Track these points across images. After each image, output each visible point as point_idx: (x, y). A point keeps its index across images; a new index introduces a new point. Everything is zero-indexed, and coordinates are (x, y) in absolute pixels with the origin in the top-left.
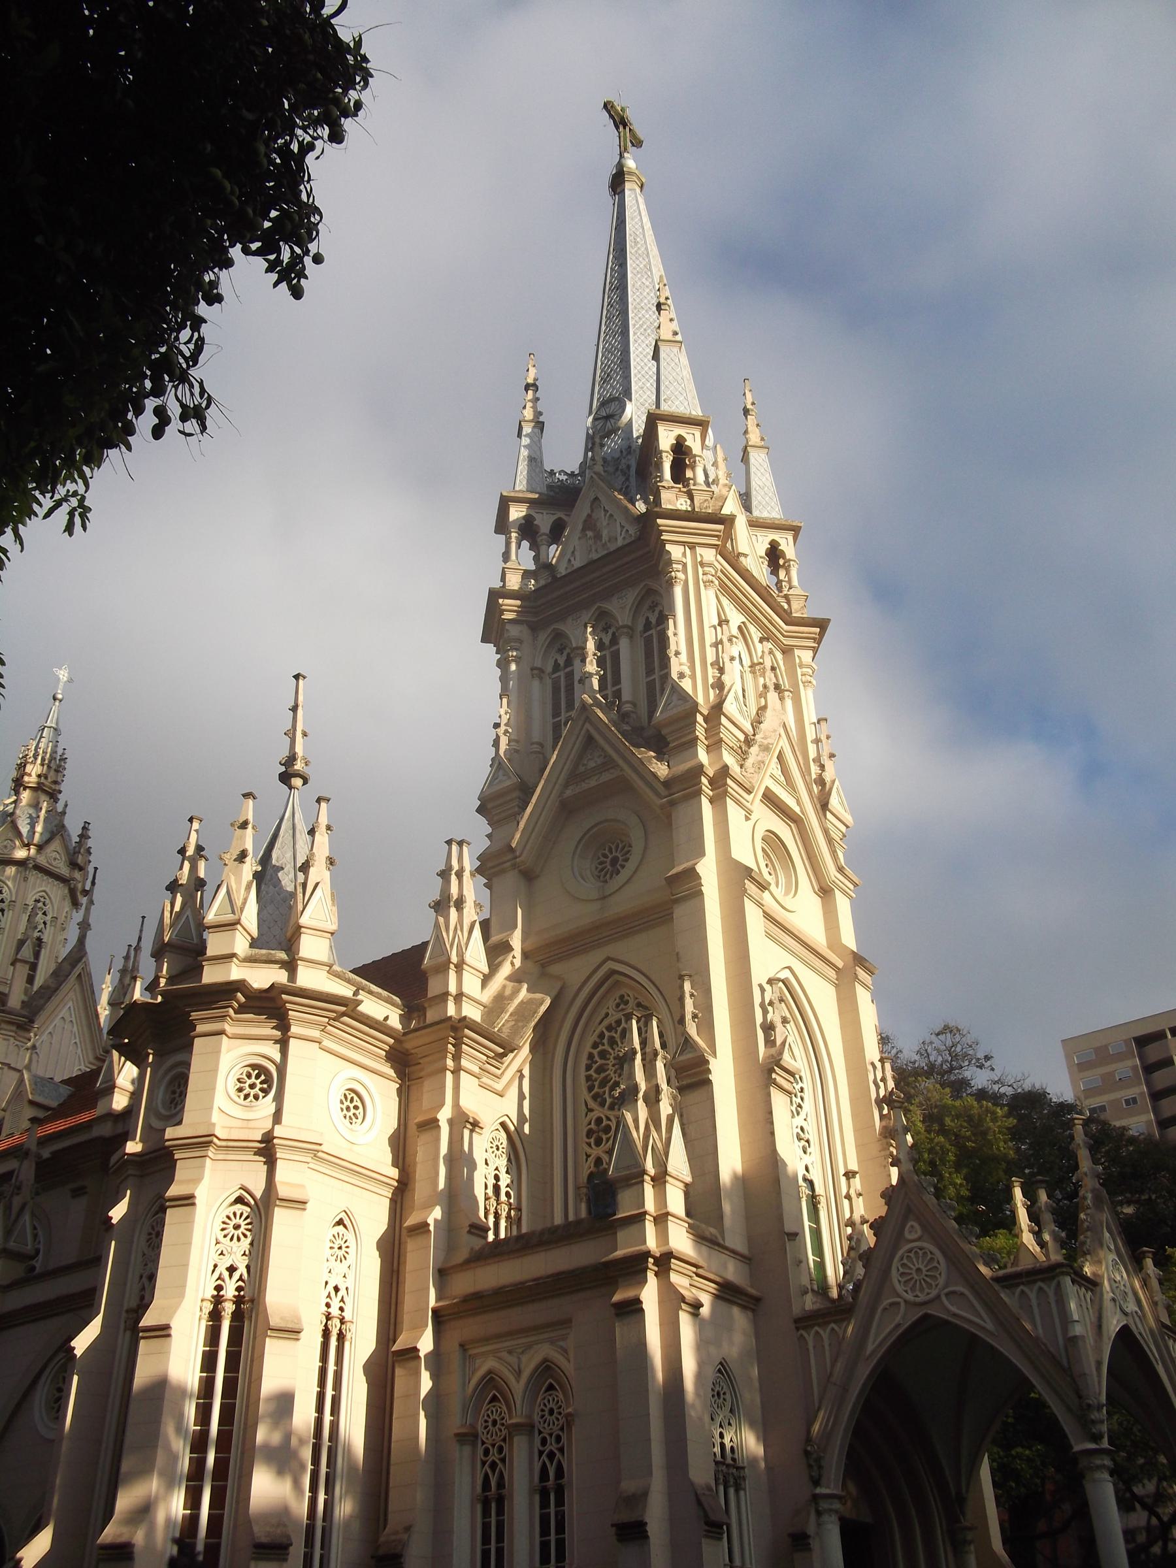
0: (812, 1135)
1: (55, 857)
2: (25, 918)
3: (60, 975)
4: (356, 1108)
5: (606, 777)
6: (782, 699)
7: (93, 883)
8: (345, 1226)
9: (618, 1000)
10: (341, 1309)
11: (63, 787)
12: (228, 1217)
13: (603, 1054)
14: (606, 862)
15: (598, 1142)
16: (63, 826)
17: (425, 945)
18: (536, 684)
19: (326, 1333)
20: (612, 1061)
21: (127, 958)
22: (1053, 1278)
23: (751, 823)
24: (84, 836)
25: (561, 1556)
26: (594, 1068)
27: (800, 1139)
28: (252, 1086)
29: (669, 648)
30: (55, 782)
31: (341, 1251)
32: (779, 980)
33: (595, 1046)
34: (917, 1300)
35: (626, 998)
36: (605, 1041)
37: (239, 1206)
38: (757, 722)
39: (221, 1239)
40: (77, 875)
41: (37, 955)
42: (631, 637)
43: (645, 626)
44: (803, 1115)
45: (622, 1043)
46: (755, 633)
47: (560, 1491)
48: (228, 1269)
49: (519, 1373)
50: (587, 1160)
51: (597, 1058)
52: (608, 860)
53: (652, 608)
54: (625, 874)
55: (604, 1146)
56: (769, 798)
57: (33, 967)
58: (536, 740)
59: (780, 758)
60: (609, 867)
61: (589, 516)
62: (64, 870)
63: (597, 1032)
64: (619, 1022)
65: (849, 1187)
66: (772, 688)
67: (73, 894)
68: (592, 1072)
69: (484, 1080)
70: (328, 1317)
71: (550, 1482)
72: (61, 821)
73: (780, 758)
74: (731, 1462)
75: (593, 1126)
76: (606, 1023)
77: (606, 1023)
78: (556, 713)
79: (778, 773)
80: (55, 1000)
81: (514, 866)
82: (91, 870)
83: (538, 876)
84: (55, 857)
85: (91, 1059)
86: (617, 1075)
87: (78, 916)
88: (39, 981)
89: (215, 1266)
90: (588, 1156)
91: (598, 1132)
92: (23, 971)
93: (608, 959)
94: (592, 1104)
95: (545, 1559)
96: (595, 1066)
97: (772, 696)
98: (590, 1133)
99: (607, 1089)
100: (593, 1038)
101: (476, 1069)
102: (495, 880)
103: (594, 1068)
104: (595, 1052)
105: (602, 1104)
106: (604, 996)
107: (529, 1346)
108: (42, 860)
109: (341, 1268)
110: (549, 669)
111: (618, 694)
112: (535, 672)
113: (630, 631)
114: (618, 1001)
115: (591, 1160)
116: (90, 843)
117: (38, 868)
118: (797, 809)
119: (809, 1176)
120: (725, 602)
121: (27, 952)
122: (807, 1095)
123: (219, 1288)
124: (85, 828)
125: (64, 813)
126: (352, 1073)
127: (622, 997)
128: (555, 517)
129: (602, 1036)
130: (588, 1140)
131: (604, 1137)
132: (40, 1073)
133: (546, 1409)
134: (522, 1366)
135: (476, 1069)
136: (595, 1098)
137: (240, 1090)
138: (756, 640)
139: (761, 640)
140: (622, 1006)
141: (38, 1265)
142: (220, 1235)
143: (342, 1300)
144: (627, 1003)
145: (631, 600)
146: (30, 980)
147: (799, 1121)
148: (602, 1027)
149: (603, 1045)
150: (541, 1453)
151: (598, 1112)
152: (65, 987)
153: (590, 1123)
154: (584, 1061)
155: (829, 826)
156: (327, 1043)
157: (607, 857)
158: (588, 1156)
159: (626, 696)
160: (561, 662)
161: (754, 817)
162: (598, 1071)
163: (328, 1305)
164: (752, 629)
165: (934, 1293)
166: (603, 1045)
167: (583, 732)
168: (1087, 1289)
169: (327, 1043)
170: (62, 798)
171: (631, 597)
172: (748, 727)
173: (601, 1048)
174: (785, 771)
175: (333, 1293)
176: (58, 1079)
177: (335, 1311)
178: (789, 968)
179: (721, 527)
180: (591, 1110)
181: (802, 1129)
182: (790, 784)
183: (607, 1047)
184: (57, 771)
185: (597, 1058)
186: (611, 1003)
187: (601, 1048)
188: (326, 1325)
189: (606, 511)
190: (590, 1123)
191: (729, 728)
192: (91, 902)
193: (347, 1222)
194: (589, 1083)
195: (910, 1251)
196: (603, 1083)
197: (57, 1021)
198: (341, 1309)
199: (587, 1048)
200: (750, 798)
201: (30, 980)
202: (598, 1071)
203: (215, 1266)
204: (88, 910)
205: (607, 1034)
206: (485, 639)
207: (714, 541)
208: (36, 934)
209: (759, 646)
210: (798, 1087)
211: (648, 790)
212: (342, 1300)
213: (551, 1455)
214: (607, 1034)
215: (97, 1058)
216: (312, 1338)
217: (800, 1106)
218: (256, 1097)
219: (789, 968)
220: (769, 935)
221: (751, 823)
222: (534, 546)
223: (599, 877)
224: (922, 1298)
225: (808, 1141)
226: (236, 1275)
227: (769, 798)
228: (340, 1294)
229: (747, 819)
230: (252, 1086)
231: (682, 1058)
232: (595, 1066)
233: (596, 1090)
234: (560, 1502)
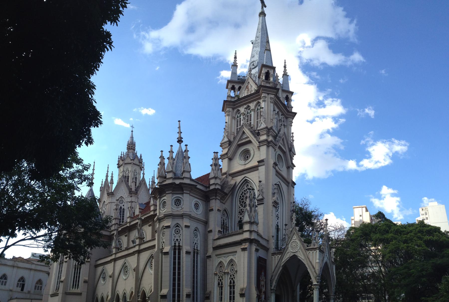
0: (279, 216)
1: (136, 161)
2: (133, 173)
3: (140, 183)
4: (197, 207)
5: (247, 140)
6: (285, 127)
7: (144, 165)
8: (197, 231)
10: (197, 248)
11: (136, 148)
12: (176, 230)
13: (243, 196)
15: (241, 214)
16: (137, 156)
17: (209, 173)
18: (233, 120)
19: (194, 253)
20: (245, 198)
21: (152, 179)
22: (316, 250)
23: (276, 152)
24: (141, 157)
25: (234, 299)
27: (277, 217)
28: (178, 203)
29: (256, 288)
30: (134, 147)
31: (196, 236)
32: (277, 184)
33: (241, 194)
34: (293, 252)
37: (177, 227)
38: (278, 133)
39: (175, 234)
40: (141, 164)
41: (136, 180)
42: (254, 112)
44: (278, 212)
46: (280, 113)
47: (234, 286)
48: (176, 240)
49: (226, 262)
51: (242, 197)
53: (259, 106)
54: (249, 160)
55: (242, 215)
56: (280, 148)
57: (136, 183)
58: (233, 132)
59: (283, 139)
61: (247, 86)
62: (138, 164)
64: (246, 190)
65: (285, 227)
66: (283, 125)
67: (140, 167)
68: (240, 200)
69: (221, 201)
70: (194, 249)
71: (232, 284)
72: (136, 155)
73: (283, 139)
75: (240, 211)
76: (244, 190)
79: (282, 142)
80: (141, 189)
81: (227, 157)
82: (143, 163)
84: (136, 161)
85: (148, 199)
87: (142, 172)
88: (137, 185)
89: (174, 239)
90: (239, 217)
92: (134, 183)
95: (230, 299)
96: (241, 199)
97: (283, 127)
98: (239, 212)
100: (241, 193)
101: (219, 199)
102: (223, 160)
104: (241, 196)
105: (242, 206)
106: (244, 185)
107: (228, 256)
108: (134, 162)
109: (196, 239)
110: (236, 117)
111: (251, 123)
112: (234, 118)
113: (254, 110)
115: (239, 218)
116: (142, 158)
117: (134, 164)
118: (285, 150)
119: (278, 224)
120: (275, 106)
121: (134, 180)
122: (280, 208)
123: (175, 244)
124: (141, 155)
125: (137, 153)
126: (195, 200)
127: (247, 185)
128: (239, 86)
129: (243, 192)
131: (242, 213)
132: (141, 202)
134: (227, 260)
135: (219, 199)
136: (241, 205)
137: (177, 205)
138: (280, 115)
139: (281, 115)
141: (145, 240)
142: (174, 233)
143: (197, 246)
145: (255, 104)
146: (136, 185)
147: (277, 213)
150: (230, 278)
152: (142, 186)
154: (239, 197)
155: (291, 154)
156: (191, 194)
158: (239, 217)
159: (252, 122)
160: (239, 116)
161: (276, 151)
163: (194, 247)
164: (280, 112)
165: (297, 251)
168: (322, 253)
169: (191, 194)
170: (136, 150)
171: (255, 103)
172: (277, 132)
173: (243, 195)
174: (283, 142)
175: (195, 245)
176: (143, 203)
177: (196, 248)
178: (279, 182)
179: (276, 91)
180: (240, 208)
181: (278, 215)
182: (284, 145)
183: (244, 195)
184: (134, 145)
185: (242, 197)
186: (245, 186)
187: (243, 195)
188: (194, 251)
189: (251, 85)
192: (144, 169)
193: (197, 230)
195: (293, 242)
196: (243, 202)
197: (141, 193)
198: (197, 248)
199: (240, 195)
200: (276, 147)
201: (136, 185)
203: (174, 239)
204: (144, 171)
208: (135, 176)
209: (281, 116)
210: (278, 206)
211: (255, 143)
212: (197, 246)
213: (232, 279)
214: (244, 192)
215: (150, 199)
216: (192, 254)
217: (278, 210)
218: (179, 205)
219: (279, 182)
220: (276, 175)
221: (276, 152)
222: (234, 92)
224: (294, 251)
225: (278, 217)
226: (178, 241)
227: (280, 148)
228: (196, 245)
229: (275, 151)
230: (178, 203)
231: (258, 198)
232: (241, 199)
233: (241, 203)
234: (234, 288)
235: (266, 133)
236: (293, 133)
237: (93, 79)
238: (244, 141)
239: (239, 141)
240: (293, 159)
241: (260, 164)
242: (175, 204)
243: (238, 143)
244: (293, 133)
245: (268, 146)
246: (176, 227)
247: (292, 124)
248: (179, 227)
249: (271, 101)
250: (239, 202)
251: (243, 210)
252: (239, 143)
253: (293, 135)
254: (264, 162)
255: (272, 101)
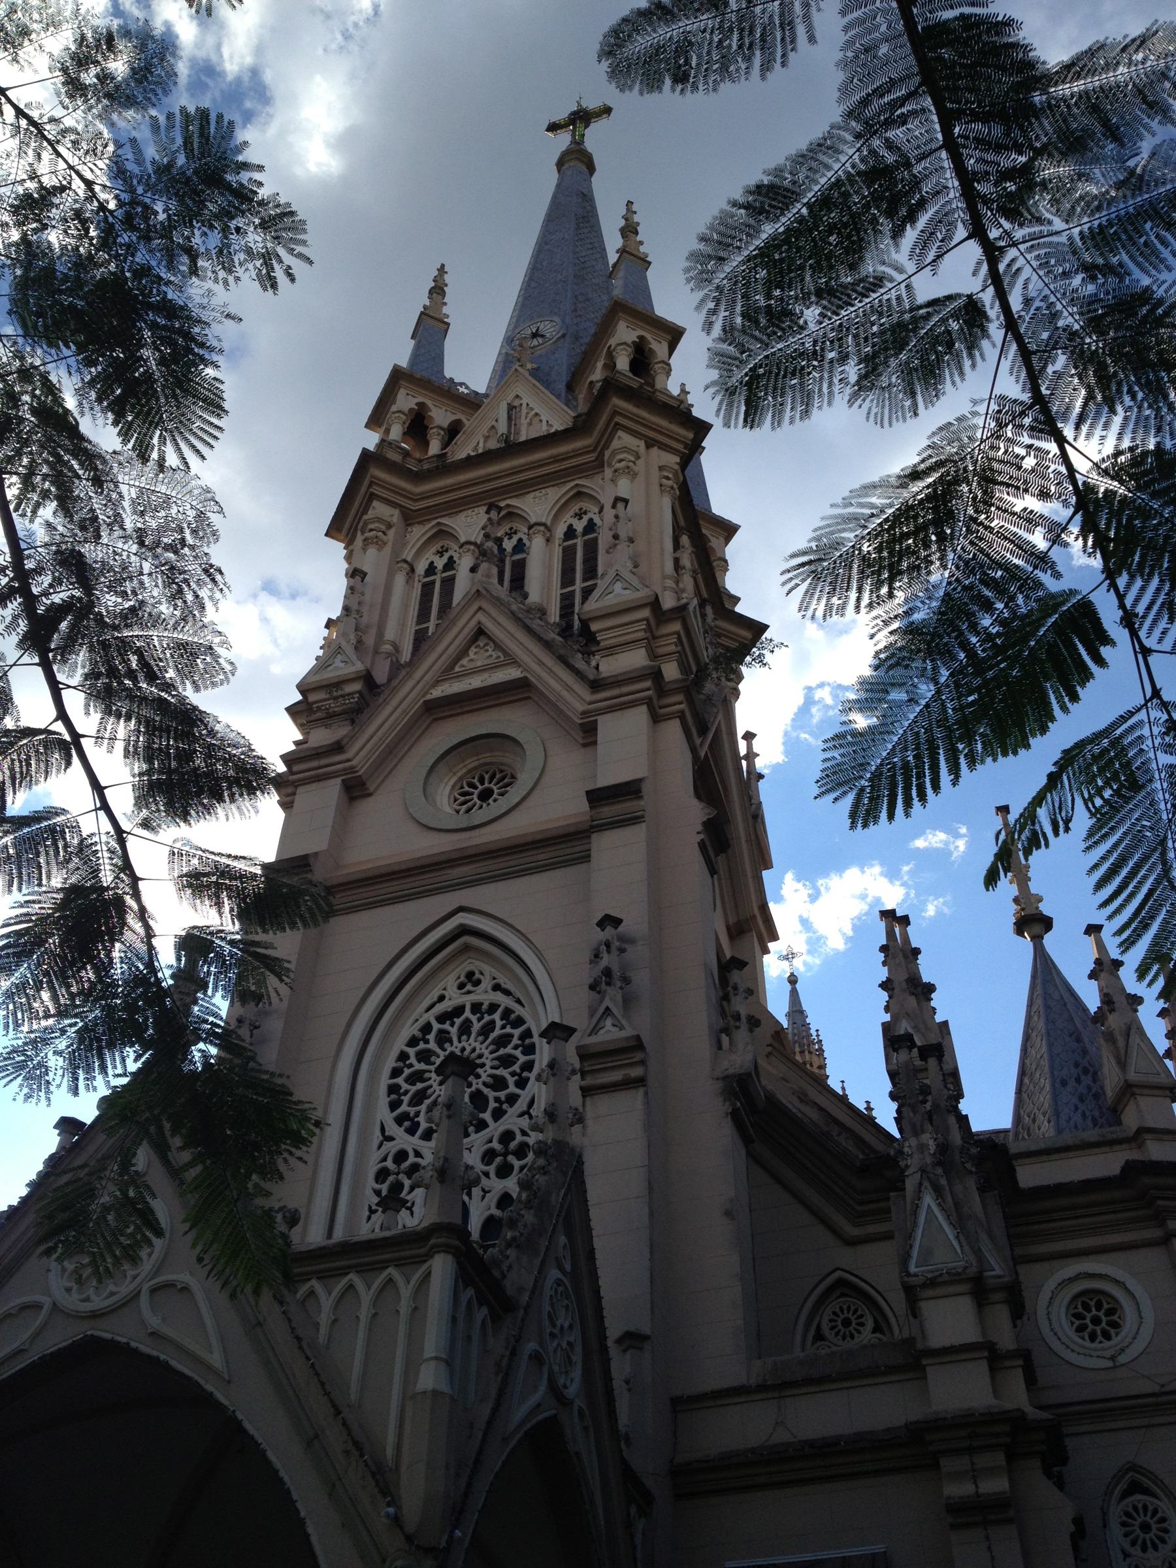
9: (462, 979)
14: (476, 788)
26: (418, 1048)
28: (1096, 1321)
33: (413, 1042)
35: (477, 976)
36: (431, 1037)
37: (1138, 1497)
43: (566, 534)
45: (460, 1042)
50: (369, 1218)
52: (476, 792)
55: (392, 1148)
60: (476, 799)
63: (421, 1022)
68: (400, 1080)
74: (505, 1269)
75: (389, 1164)
77: (440, 1008)
78: (423, 614)
83: (370, 795)
86: (478, 1051)
91: (398, 1174)
93: (461, 909)
94: (393, 1129)
99: (423, 1108)
100: (409, 1030)
103: (418, 1048)
104: (411, 1051)
114: (462, 979)
127: (470, 975)
129: (427, 1028)
130: (377, 1186)
133: (486, 785)
136: (399, 1121)
140: (469, 987)
144: (477, 983)
148: (430, 1017)
149: (427, 1042)
151: (403, 1140)
153: (384, 1159)
154: (390, 1063)
157: (476, 788)
162: (412, 1080)
166: (427, 1042)
167: (473, 623)
180: (391, 1139)
185: (511, 1081)
187: (422, 1046)
190: (384, 1159)
191: (540, 983)
194: (393, 1096)
199: (400, 1044)
202: (412, 1080)
205: (436, 1026)
206: (333, 531)
207: (680, 447)
223: (456, 800)
233: (404, 1108)
235: (641, 635)
236: (749, 736)
237: (97, 1113)
238: (476, 682)
239: (437, 683)
240: (1027, 746)
241: (608, 811)
242: (1080, 1329)
243: (426, 693)
244: (749, 736)
245: (656, 718)
246: (1125, 1494)
247: (741, 687)
248: (1147, 1492)
249: (664, 481)
250: (383, 1100)
251: (412, 1159)
252: (437, 693)
253: (750, 747)
254: (642, 803)
255: (670, 483)
